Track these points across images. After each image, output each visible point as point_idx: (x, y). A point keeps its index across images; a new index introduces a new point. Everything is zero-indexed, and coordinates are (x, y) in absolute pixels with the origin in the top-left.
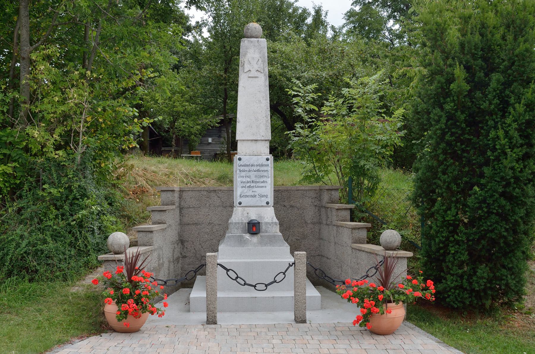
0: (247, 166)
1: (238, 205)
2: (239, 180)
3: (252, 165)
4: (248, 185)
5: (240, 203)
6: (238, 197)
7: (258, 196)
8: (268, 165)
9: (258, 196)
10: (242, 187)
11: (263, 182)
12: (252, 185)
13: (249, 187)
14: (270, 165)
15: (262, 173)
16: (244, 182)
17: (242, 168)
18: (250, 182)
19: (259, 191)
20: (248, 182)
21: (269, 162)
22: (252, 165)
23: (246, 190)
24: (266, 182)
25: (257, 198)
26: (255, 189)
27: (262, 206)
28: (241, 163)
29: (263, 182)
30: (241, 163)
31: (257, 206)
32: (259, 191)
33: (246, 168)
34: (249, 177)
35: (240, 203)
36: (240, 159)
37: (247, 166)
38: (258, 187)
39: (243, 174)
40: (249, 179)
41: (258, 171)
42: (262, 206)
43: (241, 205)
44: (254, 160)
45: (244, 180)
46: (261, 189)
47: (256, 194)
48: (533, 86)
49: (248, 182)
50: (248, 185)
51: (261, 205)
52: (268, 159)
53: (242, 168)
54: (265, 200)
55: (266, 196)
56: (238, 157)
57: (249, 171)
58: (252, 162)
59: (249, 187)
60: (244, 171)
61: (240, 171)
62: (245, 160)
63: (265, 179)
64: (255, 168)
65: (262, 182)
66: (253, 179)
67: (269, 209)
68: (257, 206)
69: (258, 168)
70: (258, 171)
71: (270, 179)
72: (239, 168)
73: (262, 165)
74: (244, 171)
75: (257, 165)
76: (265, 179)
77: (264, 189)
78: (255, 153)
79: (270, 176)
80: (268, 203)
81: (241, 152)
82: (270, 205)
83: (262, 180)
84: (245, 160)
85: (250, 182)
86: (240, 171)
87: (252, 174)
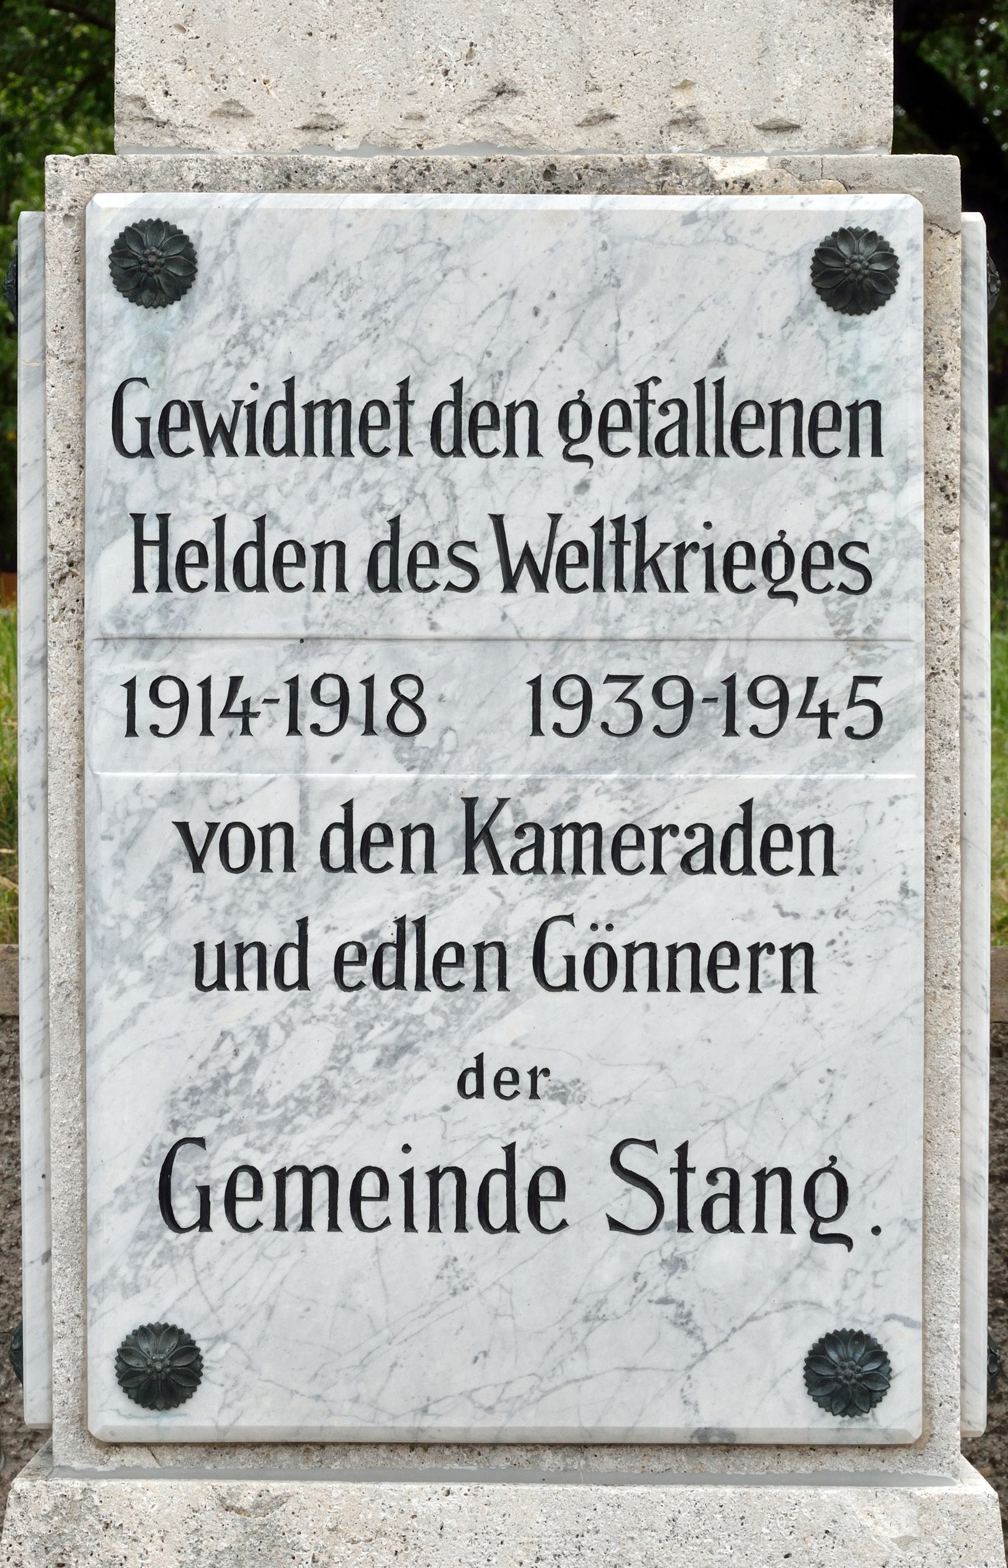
0: (345, 427)
1: (114, 1411)
2: (143, 778)
3: (467, 425)
4: (365, 906)
5: (162, 1369)
6: (122, 1221)
7: (594, 1192)
8: (861, 423)
9: (594, 1192)
10: (218, 967)
11: (739, 846)
12: (466, 907)
13: (398, 959)
14: (904, 418)
15: (700, 608)
16: (264, 847)
17: (207, 493)
18: (410, 843)
19: (631, 1065)
20: (356, 846)
21: (887, 343)
22: (467, 425)
23: (304, 1034)
24: (820, 847)
25: (587, 1253)
26: (518, 1026)
27: (713, 1449)
28: (194, 352)
29: (739, 846)
30: (194, 352)
31: (580, 1451)
32: (631, 1065)
33: (319, 499)
34: (394, 710)
35: (162, 1369)
36: (155, 267)
37: (345, 427)
38: (609, 966)
39: (240, 634)
40: (374, 778)
41: (619, 556)
42: (713, 1449)
43: (200, 1414)
44: (506, 294)
45: (264, 780)
46: (686, 1011)
47: (549, 1134)
48: (3, 1241)
49: (356, 846)
50: (365, 906)
51: (669, 1420)
52: (851, 276)
53: (207, 493)
54: (762, 1304)
55: (815, 1203)
56: (113, 212)
57: (397, 565)
58: (447, 350)
59: (398, 959)
60: (260, 563)
61: (167, 562)
62: (292, 289)
63: (778, 774)
64: (539, 494)
65: (712, 853)
66: (491, 751)
67: (876, 1515)
68: (580, 1451)
69: (617, 483)
70: (619, 556)
71: (900, 770)
72: (143, 486)
73: (714, 424)
74: (260, 563)
75: (589, 427)
76: (778, 774)
77: (752, 1017)
78: (548, 122)
79: (900, 685)
80: (846, 1373)
81: (191, 102)
82: (896, 1412)
83: (702, 785)
84: (292, 289)
85: (410, 843)
86: (167, 562)
87: (481, 648)
